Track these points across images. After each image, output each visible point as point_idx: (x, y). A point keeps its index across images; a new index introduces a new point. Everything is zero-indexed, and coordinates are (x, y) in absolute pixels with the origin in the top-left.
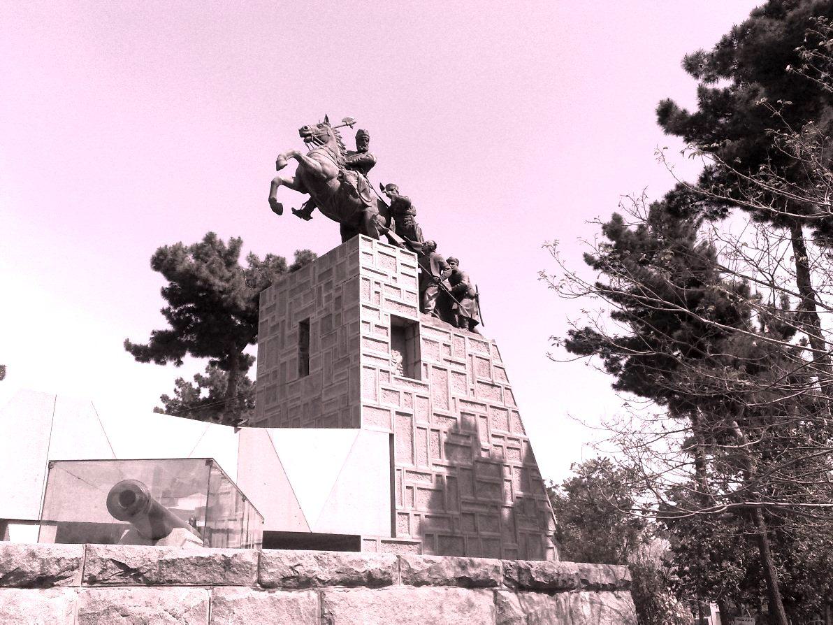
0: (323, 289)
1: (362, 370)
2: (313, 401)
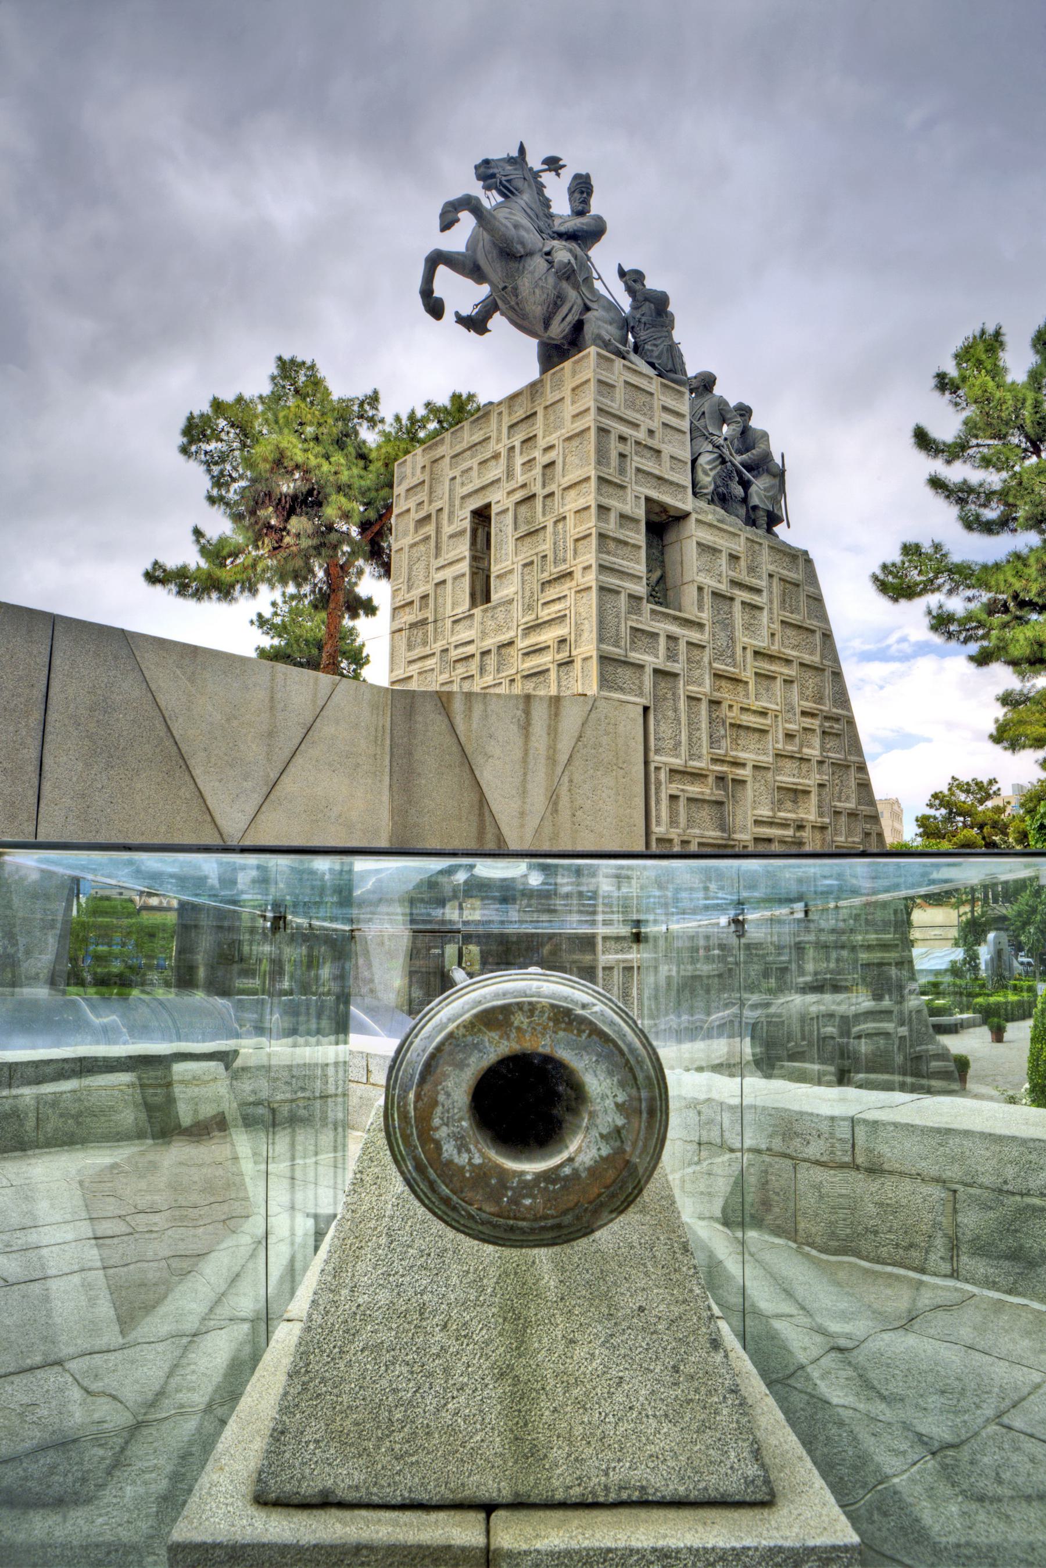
2: (502, 646)
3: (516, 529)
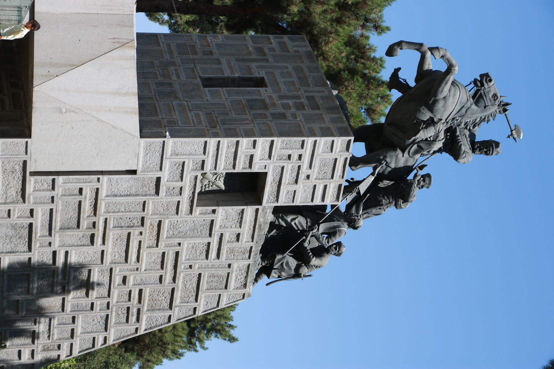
0: (298, 101)
1: (203, 140)
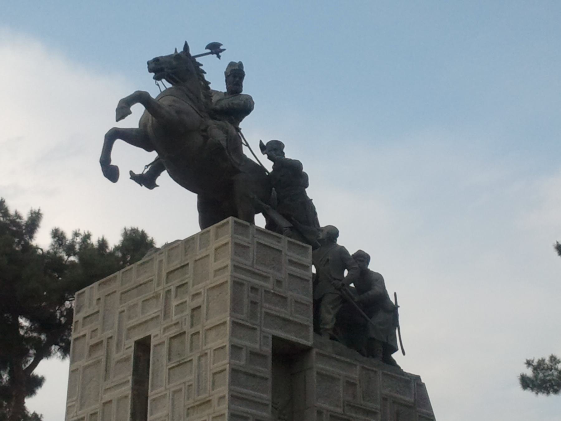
3: (170, 360)
